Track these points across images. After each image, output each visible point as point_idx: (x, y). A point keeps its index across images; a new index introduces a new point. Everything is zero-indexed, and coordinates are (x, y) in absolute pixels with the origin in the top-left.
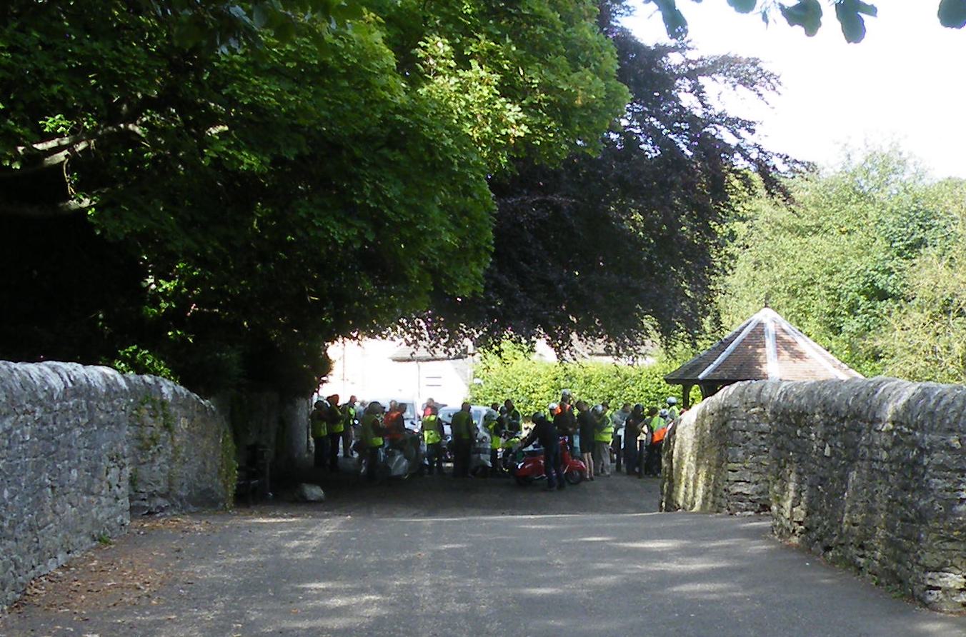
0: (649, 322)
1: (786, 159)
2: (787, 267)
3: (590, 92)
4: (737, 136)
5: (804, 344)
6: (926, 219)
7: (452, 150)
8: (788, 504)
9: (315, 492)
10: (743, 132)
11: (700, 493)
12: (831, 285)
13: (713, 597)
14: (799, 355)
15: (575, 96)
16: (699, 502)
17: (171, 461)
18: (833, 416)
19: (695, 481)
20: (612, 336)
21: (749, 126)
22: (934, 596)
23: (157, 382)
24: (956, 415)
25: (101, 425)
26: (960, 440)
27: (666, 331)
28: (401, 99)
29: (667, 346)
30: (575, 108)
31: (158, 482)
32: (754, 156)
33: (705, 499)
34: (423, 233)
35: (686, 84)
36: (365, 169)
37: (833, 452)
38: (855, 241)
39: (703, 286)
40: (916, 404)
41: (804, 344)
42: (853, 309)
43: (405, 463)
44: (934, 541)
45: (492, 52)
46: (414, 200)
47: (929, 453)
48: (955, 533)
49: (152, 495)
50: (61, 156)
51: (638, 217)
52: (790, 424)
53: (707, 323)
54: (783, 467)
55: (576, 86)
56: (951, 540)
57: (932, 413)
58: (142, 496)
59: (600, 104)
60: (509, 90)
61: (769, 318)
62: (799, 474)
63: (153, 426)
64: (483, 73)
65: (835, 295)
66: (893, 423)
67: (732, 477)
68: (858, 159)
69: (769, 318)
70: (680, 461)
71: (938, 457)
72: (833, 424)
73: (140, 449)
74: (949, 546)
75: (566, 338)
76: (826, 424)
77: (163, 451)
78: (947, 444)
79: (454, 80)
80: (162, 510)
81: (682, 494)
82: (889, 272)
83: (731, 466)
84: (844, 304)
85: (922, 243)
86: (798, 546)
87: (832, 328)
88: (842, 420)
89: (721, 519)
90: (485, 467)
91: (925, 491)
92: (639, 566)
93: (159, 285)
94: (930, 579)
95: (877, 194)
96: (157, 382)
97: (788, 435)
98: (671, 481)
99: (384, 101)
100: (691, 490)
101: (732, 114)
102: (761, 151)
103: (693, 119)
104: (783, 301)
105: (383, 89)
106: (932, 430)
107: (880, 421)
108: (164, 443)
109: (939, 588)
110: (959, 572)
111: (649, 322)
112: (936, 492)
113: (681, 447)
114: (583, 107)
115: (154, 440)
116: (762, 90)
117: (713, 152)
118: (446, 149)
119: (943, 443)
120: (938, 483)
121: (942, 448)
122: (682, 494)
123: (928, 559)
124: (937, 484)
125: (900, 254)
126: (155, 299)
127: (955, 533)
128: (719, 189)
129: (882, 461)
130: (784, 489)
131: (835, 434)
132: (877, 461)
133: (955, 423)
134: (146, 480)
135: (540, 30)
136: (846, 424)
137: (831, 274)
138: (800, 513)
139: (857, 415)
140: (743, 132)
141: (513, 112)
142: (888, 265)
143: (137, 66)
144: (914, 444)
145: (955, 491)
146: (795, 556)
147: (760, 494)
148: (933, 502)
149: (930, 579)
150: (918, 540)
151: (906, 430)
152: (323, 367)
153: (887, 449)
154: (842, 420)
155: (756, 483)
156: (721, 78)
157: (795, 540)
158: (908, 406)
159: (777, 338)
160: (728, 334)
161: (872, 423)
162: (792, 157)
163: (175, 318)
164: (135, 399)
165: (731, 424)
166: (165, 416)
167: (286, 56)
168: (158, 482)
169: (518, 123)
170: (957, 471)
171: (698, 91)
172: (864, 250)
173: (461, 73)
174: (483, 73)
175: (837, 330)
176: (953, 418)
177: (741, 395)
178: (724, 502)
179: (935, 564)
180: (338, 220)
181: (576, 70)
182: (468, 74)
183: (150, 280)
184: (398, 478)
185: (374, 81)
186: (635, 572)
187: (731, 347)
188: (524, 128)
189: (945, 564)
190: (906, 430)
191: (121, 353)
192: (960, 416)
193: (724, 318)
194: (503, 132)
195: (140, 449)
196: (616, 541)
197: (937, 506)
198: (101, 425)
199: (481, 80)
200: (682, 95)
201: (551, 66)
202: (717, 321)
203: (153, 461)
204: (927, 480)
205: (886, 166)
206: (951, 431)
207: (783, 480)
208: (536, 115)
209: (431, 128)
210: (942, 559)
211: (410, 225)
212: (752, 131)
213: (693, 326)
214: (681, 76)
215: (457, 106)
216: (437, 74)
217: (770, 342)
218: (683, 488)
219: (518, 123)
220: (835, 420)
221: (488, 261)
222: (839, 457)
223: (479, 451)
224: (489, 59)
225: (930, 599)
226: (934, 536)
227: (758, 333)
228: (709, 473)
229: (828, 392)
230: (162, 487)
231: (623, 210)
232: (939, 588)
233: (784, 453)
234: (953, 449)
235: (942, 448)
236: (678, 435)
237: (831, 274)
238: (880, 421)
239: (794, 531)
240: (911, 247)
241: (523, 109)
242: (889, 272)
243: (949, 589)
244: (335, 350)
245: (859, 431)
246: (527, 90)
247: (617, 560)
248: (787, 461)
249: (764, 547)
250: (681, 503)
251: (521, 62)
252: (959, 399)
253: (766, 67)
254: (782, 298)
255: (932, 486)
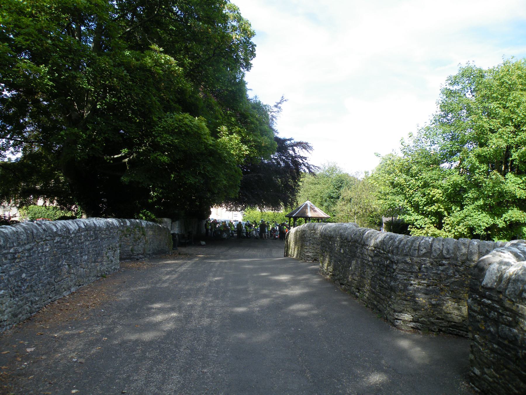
0: (282, 204)
1: (314, 166)
2: (312, 192)
3: (266, 142)
4: (302, 160)
5: (316, 209)
6: (342, 182)
7: (226, 157)
8: (326, 265)
9: (203, 243)
10: (304, 160)
11: (296, 253)
12: (321, 195)
13: (304, 314)
14: (315, 211)
15: (262, 143)
16: (295, 255)
17: (144, 244)
18: (345, 240)
19: (294, 249)
20: (273, 206)
21: (305, 158)
22: (399, 323)
23: (141, 222)
24: (408, 249)
25: (102, 239)
26: (411, 259)
27: (286, 206)
28: (211, 142)
29: (286, 209)
30: (262, 147)
31: (140, 251)
32: (306, 165)
33: (297, 255)
34: (218, 180)
35: (291, 148)
36: (200, 162)
37: (344, 252)
38: (326, 186)
39: (294, 195)
40: (388, 243)
41: (316, 209)
42: (326, 201)
43: (226, 235)
44: (399, 300)
45: (240, 131)
46: (216, 171)
47: (396, 264)
48: (409, 298)
49: (138, 254)
50: (126, 160)
51: (279, 180)
52: (327, 239)
53: (295, 204)
54: (324, 253)
55: (262, 141)
56: (406, 300)
57: (397, 247)
58: (135, 255)
59: (269, 146)
60: (244, 141)
61: (308, 203)
62: (330, 256)
63: (138, 234)
64: (236, 136)
65: (322, 197)
66: (375, 248)
67: (306, 250)
68: (327, 168)
69: (308, 203)
70: (290, 242)
71: (401, 266)
72: (345, 243)
73: (135, 241)
74: (405, 302)
75: (263, 207)
76: (342, 242)
77: (142, 241)
78: (405, 261)
79: (228, 138)
80: (141, 258)
81: (290, 252)
82: (334, 193)
83: (305, 247)
84: (324, 199)
85: (341, 187)
86: (329, 280)
87: (321, 205)
88: (349, 242)
89: (301, 263)
90: (244, 236)
91: (395, 279)
92: (278, 292)
93: (154, 194)
94: (397, 315)
95: (331, 176)
96: (141, 222)
97: (326, 243)
98: (287, 247)
99: (205, 142)
100: (293, 251)
101: (301, 156)
102: (308, 164)
103: (292, 156)
104: (310, 199)
105: (205, 139)
106: (398, 254)
107: (367, 245)
108: (142, 239)
109: (401, 320)
110: (409, 314)
111: (282, 204)
112: (400, 280)
113: (290, 240)
114: (264, 147)
115: (139, 239)
116: (308, 150)
117: (297, 165)
118: (225, 157)
119: (403, 260)
120: (400, 276)
121: (403, 262)
122: (290, 252)
123: (395, 306)
124: (400, 277)
125: (336, 189)
126: (152, 198)
127: (409, 298)
128: (298, 173)
129: (368, 261)
130: (324, 260)
131: (346, 246)
132: (366, 260)
133: (408, 252)
134: (136, 250)
135: (253, 126)
136: (350, 243)
137: (321, 193)
138: (331, 269)
139: (356, 241)
140: (304, 160)
141: (244, 147)
142: (334, 191)
143: (132, 129)
144: (387, 258)
145: (409, 280)
146: (329, 285)
147: (314, 256)
148: (398, 284)
149: (397, 315)
150: (390, 297)
151: (383, 252)
152: (210, 213)
153: (372, 257)
154: (349, 242)
155: (313, 253)
156: (299, 147)
157: (328, 277)
158: (383, 242)
159: (310, 207)
160: (299, 206)
161: (363, 245)
162: (315, 166)
163: (158, 202)
164: (133, 227)
165: (305, 235)
166: (143, 231)
167: (175, 128)
168: (140, 251)
169: (246, 150)
170: (409, 272)
171: (294, 150)
172: (328, 188)
173: (230, 136)
174: (236, 136)
175: (322, 205)
176: (407, 250)
177: (309, 227)
178: (303, 257)
179: (399, 310)
180: (193, 176)
181: (263, 136)
182: (232, 136)
183: (152, 193)
184: (225, 238)
185: (202, 136)
186: (277, 296)
187: (300, 209)
188: (248, 152)
189: (404, 310)
190: (383, 252)
191: (141, 212)
192: (410, 249)
193: (298, 203)
194: (242, 153)
195: (135, 241)
196: (271, 275)
197: (400, 286)
198: (102, 239)
199: (236, 138)
200: (290, 151)
201: (256, 135)
202: (297, 203)
203: (139, 244)
204: (396, 275)
205: (332, 170)
206: (407, 255)
207: (324, 257)
208: (252, 149)
209: (220, 150)
210: (403, 308)
211: (214, 178)
212: (306, 159)
213: (292, 205)
214: (289, 147)
215: (229, 146)
216: (223, 136)
217: (309, 208)
218: (291, 250)
219: (246, 150)
220: (346, 241)
221: (239, 189)
222: (347, 254)
223: (243, 232)
224: (239, 133)
225: (397, 324)
226: (399, 298)
227: (306, 206)
228: (298, 249)
229: (342, 231)
230: (142, 251)
231: (277, 178)
232: (401, 320)
233: (324, 248)
234: (407, 263)
235: (403, 262)
236: (289, 236)
237: (321, 193)
238: (367, 245)
239: (328, 274)
240: (338, 187)
241: (248, 147)
242: (334, 193)
243: (406, 321)
244: (212, 209)
245: (357, 247)
246: (249, 141)
247: (271, 288)
248: (325, 251)
249: (317, 280)
250: (290, 253)
251: (248, 134)
252: (409, 242)
253: (309, 145)
254: (310, 198)
255: (398, 278)
